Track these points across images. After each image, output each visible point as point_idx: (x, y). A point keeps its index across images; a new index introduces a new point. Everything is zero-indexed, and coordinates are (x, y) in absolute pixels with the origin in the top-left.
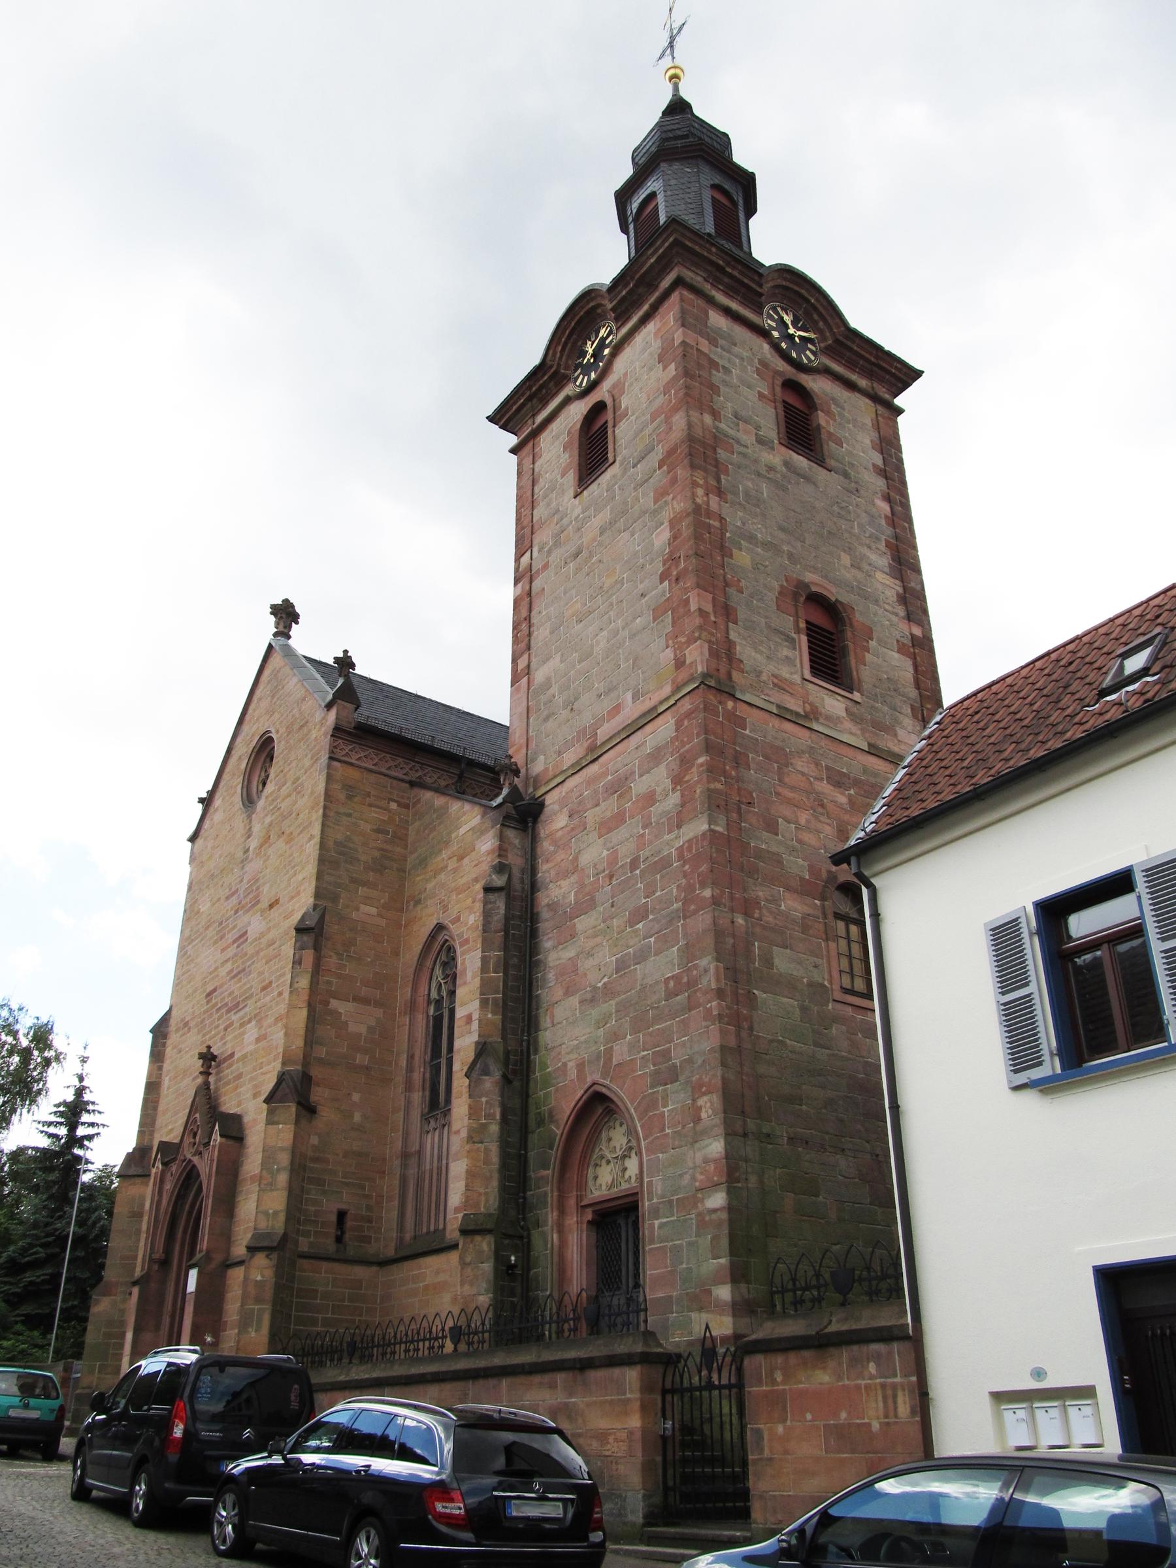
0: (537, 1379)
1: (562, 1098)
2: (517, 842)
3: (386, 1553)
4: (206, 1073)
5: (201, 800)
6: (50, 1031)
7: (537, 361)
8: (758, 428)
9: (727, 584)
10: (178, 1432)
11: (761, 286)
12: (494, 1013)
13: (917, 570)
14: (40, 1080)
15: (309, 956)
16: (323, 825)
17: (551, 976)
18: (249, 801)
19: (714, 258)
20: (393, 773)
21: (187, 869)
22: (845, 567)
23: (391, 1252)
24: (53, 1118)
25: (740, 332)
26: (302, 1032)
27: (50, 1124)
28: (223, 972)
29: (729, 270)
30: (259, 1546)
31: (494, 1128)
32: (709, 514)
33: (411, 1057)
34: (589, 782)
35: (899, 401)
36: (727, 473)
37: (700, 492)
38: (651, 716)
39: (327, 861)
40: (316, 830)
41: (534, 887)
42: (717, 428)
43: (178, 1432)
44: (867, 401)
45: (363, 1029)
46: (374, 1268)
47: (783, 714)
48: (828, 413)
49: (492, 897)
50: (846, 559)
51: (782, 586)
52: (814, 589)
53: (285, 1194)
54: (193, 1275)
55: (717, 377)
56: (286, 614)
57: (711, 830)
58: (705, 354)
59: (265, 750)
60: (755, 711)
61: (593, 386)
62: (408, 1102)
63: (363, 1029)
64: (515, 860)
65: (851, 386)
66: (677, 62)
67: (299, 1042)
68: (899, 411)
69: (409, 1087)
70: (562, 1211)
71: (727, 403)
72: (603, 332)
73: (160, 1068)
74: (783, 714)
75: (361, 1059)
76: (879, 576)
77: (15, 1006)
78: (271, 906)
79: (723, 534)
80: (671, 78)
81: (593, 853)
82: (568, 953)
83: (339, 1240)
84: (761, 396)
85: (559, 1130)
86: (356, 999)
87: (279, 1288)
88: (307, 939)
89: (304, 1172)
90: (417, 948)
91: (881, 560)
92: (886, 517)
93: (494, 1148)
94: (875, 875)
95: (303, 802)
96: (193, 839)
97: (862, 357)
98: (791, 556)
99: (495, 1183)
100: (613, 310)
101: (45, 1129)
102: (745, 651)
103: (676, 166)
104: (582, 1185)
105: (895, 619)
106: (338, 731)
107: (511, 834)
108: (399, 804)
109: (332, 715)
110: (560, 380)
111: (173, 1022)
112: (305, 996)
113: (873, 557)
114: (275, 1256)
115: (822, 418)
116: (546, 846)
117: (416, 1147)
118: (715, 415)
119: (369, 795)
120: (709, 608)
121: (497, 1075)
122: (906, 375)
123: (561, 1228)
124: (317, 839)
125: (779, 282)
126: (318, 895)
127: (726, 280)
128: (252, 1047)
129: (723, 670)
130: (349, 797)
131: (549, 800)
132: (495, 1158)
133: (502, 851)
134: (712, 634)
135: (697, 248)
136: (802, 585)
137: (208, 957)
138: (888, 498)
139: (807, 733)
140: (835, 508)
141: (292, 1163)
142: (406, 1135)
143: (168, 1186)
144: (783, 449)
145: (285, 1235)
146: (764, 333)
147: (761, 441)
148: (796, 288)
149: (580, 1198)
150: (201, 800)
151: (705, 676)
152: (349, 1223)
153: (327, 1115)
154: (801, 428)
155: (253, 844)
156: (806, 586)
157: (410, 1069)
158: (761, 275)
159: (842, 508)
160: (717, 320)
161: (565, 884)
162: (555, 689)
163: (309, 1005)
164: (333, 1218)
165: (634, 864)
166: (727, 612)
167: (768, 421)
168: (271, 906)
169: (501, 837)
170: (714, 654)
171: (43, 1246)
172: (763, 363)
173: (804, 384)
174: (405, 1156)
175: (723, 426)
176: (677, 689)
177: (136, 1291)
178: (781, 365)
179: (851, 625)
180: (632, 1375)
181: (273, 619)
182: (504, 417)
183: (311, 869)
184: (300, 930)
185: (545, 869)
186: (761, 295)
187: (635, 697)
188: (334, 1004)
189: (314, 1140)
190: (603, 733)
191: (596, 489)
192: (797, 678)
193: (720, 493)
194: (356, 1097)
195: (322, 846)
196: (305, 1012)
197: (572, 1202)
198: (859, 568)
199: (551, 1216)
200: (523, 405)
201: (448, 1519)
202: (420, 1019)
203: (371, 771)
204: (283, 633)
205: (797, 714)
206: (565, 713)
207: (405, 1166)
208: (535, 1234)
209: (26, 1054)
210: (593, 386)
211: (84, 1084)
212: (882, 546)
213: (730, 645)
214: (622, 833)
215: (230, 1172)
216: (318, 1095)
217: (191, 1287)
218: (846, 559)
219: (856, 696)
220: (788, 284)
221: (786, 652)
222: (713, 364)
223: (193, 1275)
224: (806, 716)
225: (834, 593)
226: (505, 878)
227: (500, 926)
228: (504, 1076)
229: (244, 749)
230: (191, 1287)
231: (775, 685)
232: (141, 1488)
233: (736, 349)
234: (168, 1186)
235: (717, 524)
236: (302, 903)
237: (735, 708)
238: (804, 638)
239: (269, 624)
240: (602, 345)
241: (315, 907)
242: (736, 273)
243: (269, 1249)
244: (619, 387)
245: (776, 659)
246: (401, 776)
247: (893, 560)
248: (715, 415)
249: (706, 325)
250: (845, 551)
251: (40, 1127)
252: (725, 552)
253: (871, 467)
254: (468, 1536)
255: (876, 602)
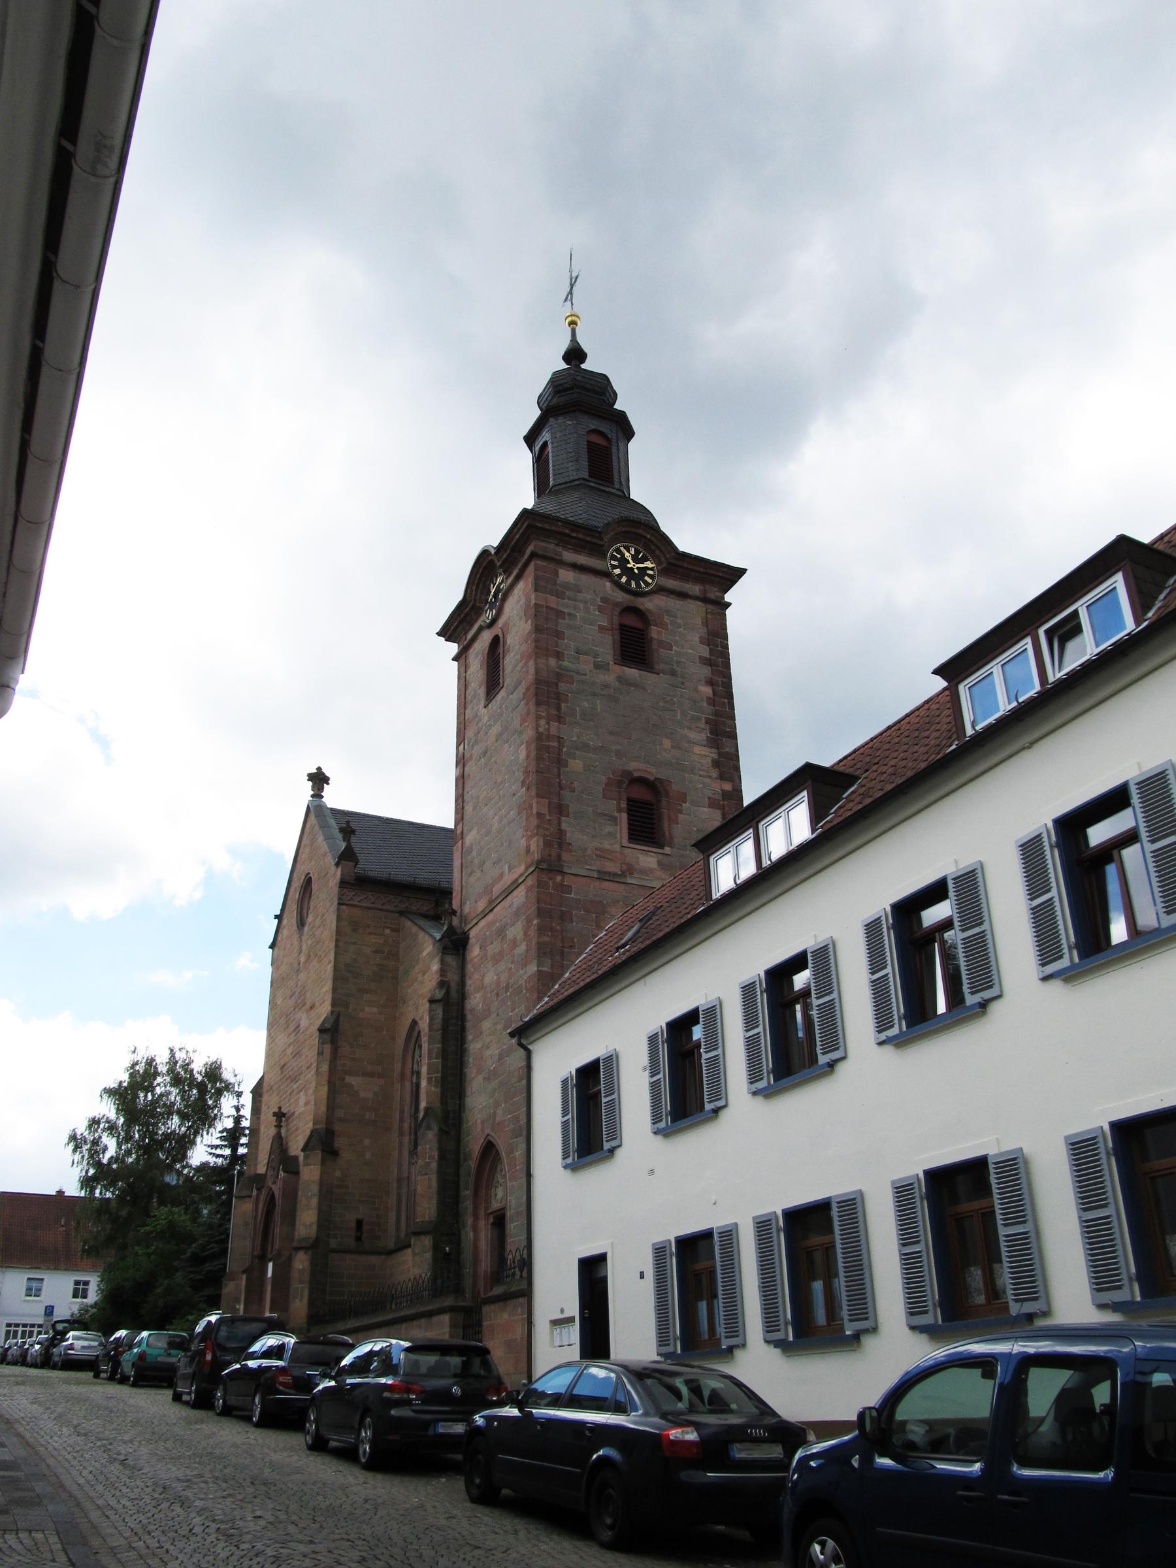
0: (415, 1323)
1: (474, 1146)
2: (454, 964)
3: (848, 1552)
4: (279, 1126)
5: (276, 917)
6: (220, 1067)
7: (460, 597)
8: (596, 655)
9: (561, 788)
10: (209, 1357)
11: (602, 539)
12: (436, 1087)
13: (733, 736)
14: (216, 1106)
15: (328, 1048)
16: (336, 953)
17: (471, 1060)
18: (301, 923)
19: (560, 530)
20: (387, 907)
21: (269, 969)
22: (666, 750)
23: (391, 1245)
24: (218, 1142)
25: (586, 579)
26: (325, 1102)
27: (217, 1147)
28: (289, 1051)
29: (574, 535)
30: (505, 1491)
31: (434, 1165)
32: (549, 738)
33: (402, 1112)
34: (489, 926)
35: (728, 597)
36: (567, 701)
37: (543, 722)
38: (515, 885)
39: (340, 977)
40: (332, 956)
41: (463, 996)
42: (560, 667)
43: (209, 1357)
44: (700, 603)
45: (370, 1095)
46: (383, 1257)
47: (603, 876)
48: (663, 625)
49: (434, 1006)
50: (667, 743)
51: (609, 778)
52: (636, 775)
53: (316, 1212)
54: (270, 1265)
55: (562, 624)
56: (319, 779)
57: (538, 971)
58: (553, 609)
59: (308, 882)
60: (579, 879)
61: (494, 621)
62: (401, 1144)
63: (370, 1095)
64: (452, 977)
65: (683, 595)
66: (576, 310)
67: (323, 1109)
68: (728, 605)
69: (401, 1134)
70: (476, 1217)
71: (569, 645)
72: (499, 580)
73: (259, 1119)
74: (603, 876)
75: (370, 1115)
76: (697, 750)
77: (190, 1050)
78: (311, 1008)
79: (560, 750)
80: (571, 323)
81: (490, 977)
82: (478, 1045)
83: (359, 1239)
84: (601, 628)
85: (473, 1164)
86: (365, 1074)
87: (313, 1273)
88: (327, 1037)
89: (328, 1194)
90: (404, 1034)
91: (699, 735)
92: (708, 698)
93: (434, 1178)
94: (531, 1043)
95: (326, 933)
96: (272, 946)
97: (692, 570)
98: (619, 754)
99: (435, 1201)
100: (501, 567)
101: (213, 1151)
102: (575, 835)
103: (561, 420)
104: (488, 1201)
105: (708, 780)
106: (343, 883)
107: (450, 959)
108: (392, 930)
109: (339, 870)
110: (479, 612)
111: (265, 1085)
112: (326, 1077)
113: (692, 735)
114: (310, 1252)
115: (654, 632)
116: (469, 968)
117: (406, 1175)
118: (559, 656)
119: (368, 926)
120: (545, 811)
121: (435, 1129)
122: (731, 575)
123: (475, 1228)
124: (332, 964)
125: (619, 529)
126: (333, 1004)
127: (573, 541)
128: (302, 1109)
129: (554, 854)
130: (355, 930)
131: (472, 934)
132: (434, 1184)
133: (443, 972)
134: (547, 829)
135: (546, 526)
136: (627, 774)
137: (282, 1039)
138: (710, 682)
139: (623, 886)
140: (661, 704)
141: (320, 1190)
142: (400, 1165)
143: (261, 1205)
144: (617, 667)
145: (317, 1238)
146: (607, 575)
147: (597, 666)
148: (634, 530)
149: (486, 1208)
150: (276, 917)
151: (539, 862)
152: (365, 1227)
153: (346, 1155)
154: (635, 644)
155: (303, 959)
156: (630, 773)
157: (402, 1120)
158: (600, 533)
159: (666, 702)
160: (566, 575)
161: (478, 996)
162: (474, 853)
163: (329, 1082)
164: (353, 1225)
165: (507, 988)
166: (560, 810)
167: (606, 647)
168: (311, 1008)
169: (442, 962)
170: (547, 844)
171: (216, 1242)
172: (605, 600)
173: (641, 607)
174: (400, 1180)
175: (566, 663)
176: (527, 868)
177: (244, 1277)
178: (620, 597)
179: (667, 795)
180: (446, 1318)
181: (310, 783)
182: (448, 632)
183: (328, 986)
184: (322, 1030)
185: (470, 983)
186: (602, 546)
187: (510, 869)
188: (348, 1079)
189: (338, 1174)
190: (497, 889)
191: (494, 704)
192: (617, 847)
193: (559, 719)
194: (367, 1142)
195: (336, 968)
196: (326, 1088)
197: (482, 1212)
198: (679, 748)
199: (469, 1221)
200: (457, 627)
201: (282, 1384)
202: (408, 1084)
203: (370, 908)
204: (317, 795)
205: (615, 875)
206: (478, 873)
207: (399, 1187)
208: (463, 1232)
209: (202, 1087)
210: (494, 621)
211: (241, 1113)
212: (702, 725)
213: (561, 833)
214: (502, 966)
215: (291, 1195)
216: (340, 1143)
217: (270, 1274)
218: (667, 743)
219: (667, 850)
220: (627, 529)
221: (609, 829)
222: (560, 614)
223: (270, 1265)
224: (623, 874)
225: (652, 773)
226: (443, 991)
227: (439, 1026)
228: (441, 1130)
229: (297, 884)
230: (270, 1274)
231: (597, 856)
232: (366, 1434)
233: (580, 596)
234: (261, 1205)
235: (555, 744)
236: (325, 1009)
237: (563, 880)
238: (624, 816)
239: (307, 788)
240: (498, 590)
241: (332, 1012)
242: (581, 536)
243: (306, 1249)
244: (506, 624)
245: (601, 835)
246: (392, 908)
247: (711, 733)
248: (559, 656)
249: (555, 583)
250: (667, 737)
251: (209, 1150)
252: (560, 762)
253: (697, 660)
254: (293, 1392)
255: (692, 771)
